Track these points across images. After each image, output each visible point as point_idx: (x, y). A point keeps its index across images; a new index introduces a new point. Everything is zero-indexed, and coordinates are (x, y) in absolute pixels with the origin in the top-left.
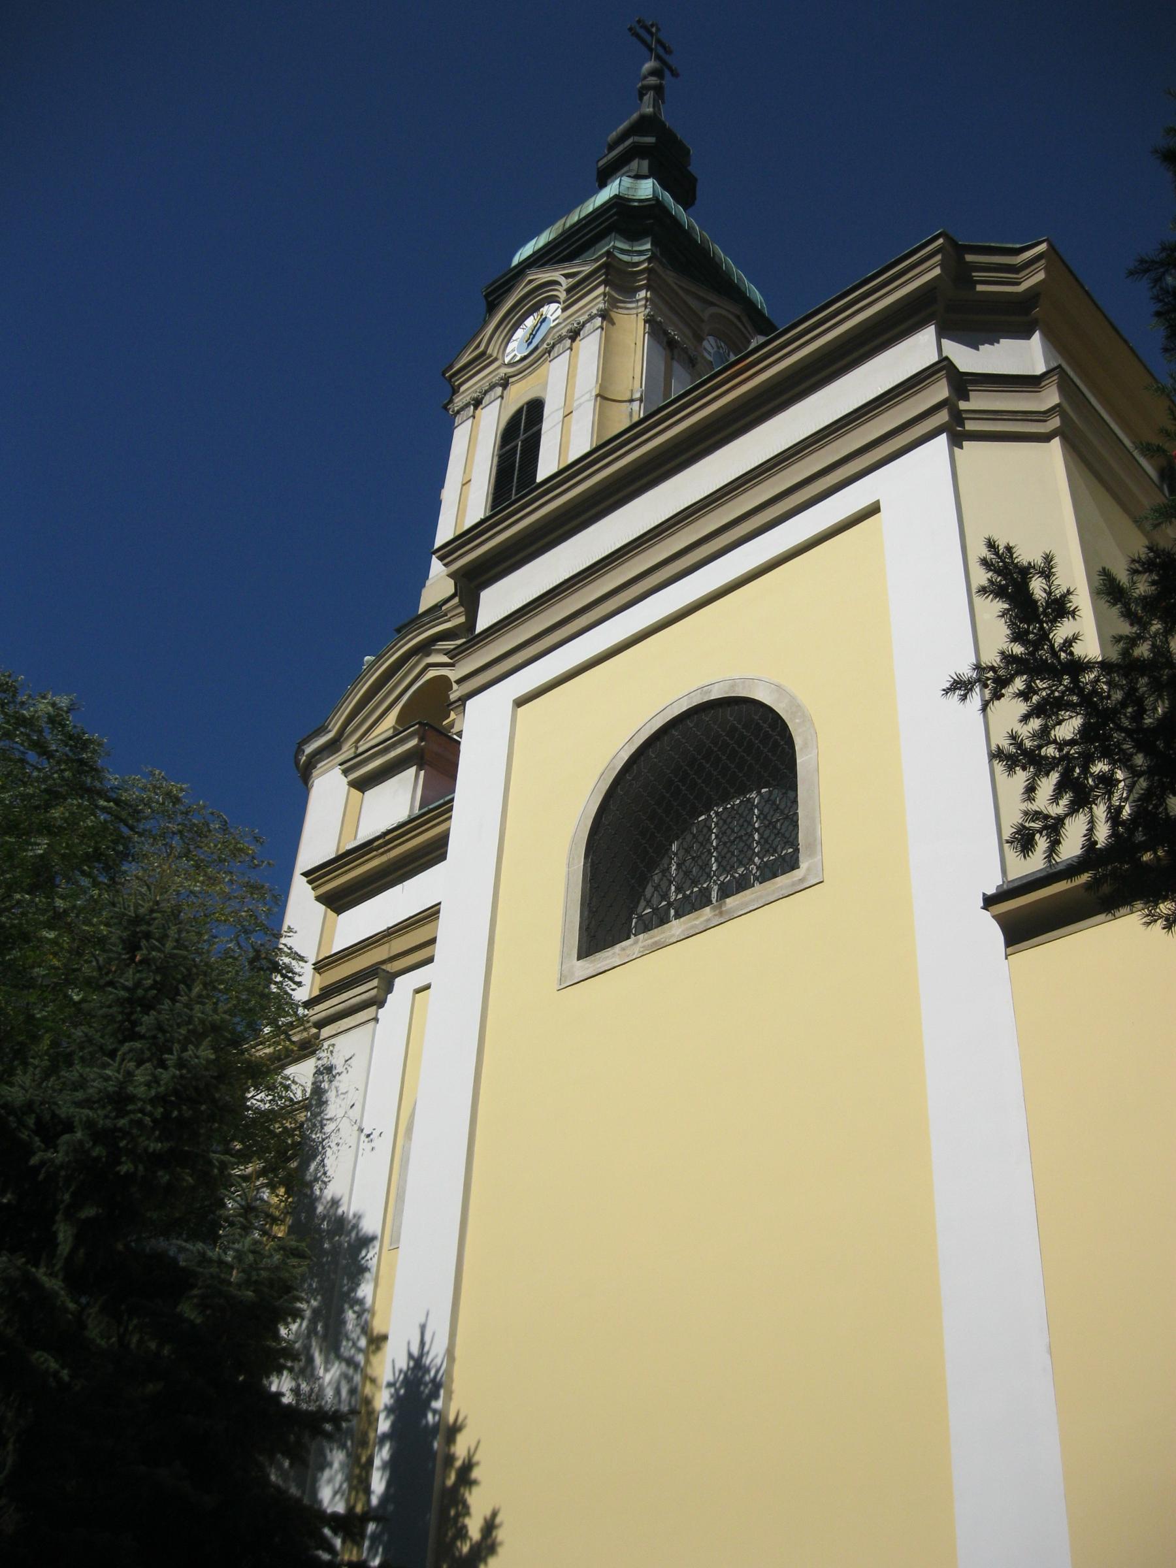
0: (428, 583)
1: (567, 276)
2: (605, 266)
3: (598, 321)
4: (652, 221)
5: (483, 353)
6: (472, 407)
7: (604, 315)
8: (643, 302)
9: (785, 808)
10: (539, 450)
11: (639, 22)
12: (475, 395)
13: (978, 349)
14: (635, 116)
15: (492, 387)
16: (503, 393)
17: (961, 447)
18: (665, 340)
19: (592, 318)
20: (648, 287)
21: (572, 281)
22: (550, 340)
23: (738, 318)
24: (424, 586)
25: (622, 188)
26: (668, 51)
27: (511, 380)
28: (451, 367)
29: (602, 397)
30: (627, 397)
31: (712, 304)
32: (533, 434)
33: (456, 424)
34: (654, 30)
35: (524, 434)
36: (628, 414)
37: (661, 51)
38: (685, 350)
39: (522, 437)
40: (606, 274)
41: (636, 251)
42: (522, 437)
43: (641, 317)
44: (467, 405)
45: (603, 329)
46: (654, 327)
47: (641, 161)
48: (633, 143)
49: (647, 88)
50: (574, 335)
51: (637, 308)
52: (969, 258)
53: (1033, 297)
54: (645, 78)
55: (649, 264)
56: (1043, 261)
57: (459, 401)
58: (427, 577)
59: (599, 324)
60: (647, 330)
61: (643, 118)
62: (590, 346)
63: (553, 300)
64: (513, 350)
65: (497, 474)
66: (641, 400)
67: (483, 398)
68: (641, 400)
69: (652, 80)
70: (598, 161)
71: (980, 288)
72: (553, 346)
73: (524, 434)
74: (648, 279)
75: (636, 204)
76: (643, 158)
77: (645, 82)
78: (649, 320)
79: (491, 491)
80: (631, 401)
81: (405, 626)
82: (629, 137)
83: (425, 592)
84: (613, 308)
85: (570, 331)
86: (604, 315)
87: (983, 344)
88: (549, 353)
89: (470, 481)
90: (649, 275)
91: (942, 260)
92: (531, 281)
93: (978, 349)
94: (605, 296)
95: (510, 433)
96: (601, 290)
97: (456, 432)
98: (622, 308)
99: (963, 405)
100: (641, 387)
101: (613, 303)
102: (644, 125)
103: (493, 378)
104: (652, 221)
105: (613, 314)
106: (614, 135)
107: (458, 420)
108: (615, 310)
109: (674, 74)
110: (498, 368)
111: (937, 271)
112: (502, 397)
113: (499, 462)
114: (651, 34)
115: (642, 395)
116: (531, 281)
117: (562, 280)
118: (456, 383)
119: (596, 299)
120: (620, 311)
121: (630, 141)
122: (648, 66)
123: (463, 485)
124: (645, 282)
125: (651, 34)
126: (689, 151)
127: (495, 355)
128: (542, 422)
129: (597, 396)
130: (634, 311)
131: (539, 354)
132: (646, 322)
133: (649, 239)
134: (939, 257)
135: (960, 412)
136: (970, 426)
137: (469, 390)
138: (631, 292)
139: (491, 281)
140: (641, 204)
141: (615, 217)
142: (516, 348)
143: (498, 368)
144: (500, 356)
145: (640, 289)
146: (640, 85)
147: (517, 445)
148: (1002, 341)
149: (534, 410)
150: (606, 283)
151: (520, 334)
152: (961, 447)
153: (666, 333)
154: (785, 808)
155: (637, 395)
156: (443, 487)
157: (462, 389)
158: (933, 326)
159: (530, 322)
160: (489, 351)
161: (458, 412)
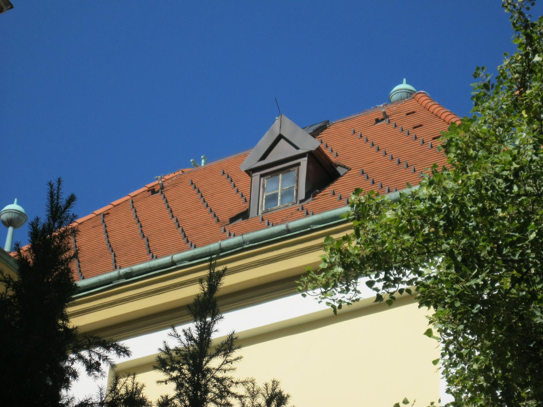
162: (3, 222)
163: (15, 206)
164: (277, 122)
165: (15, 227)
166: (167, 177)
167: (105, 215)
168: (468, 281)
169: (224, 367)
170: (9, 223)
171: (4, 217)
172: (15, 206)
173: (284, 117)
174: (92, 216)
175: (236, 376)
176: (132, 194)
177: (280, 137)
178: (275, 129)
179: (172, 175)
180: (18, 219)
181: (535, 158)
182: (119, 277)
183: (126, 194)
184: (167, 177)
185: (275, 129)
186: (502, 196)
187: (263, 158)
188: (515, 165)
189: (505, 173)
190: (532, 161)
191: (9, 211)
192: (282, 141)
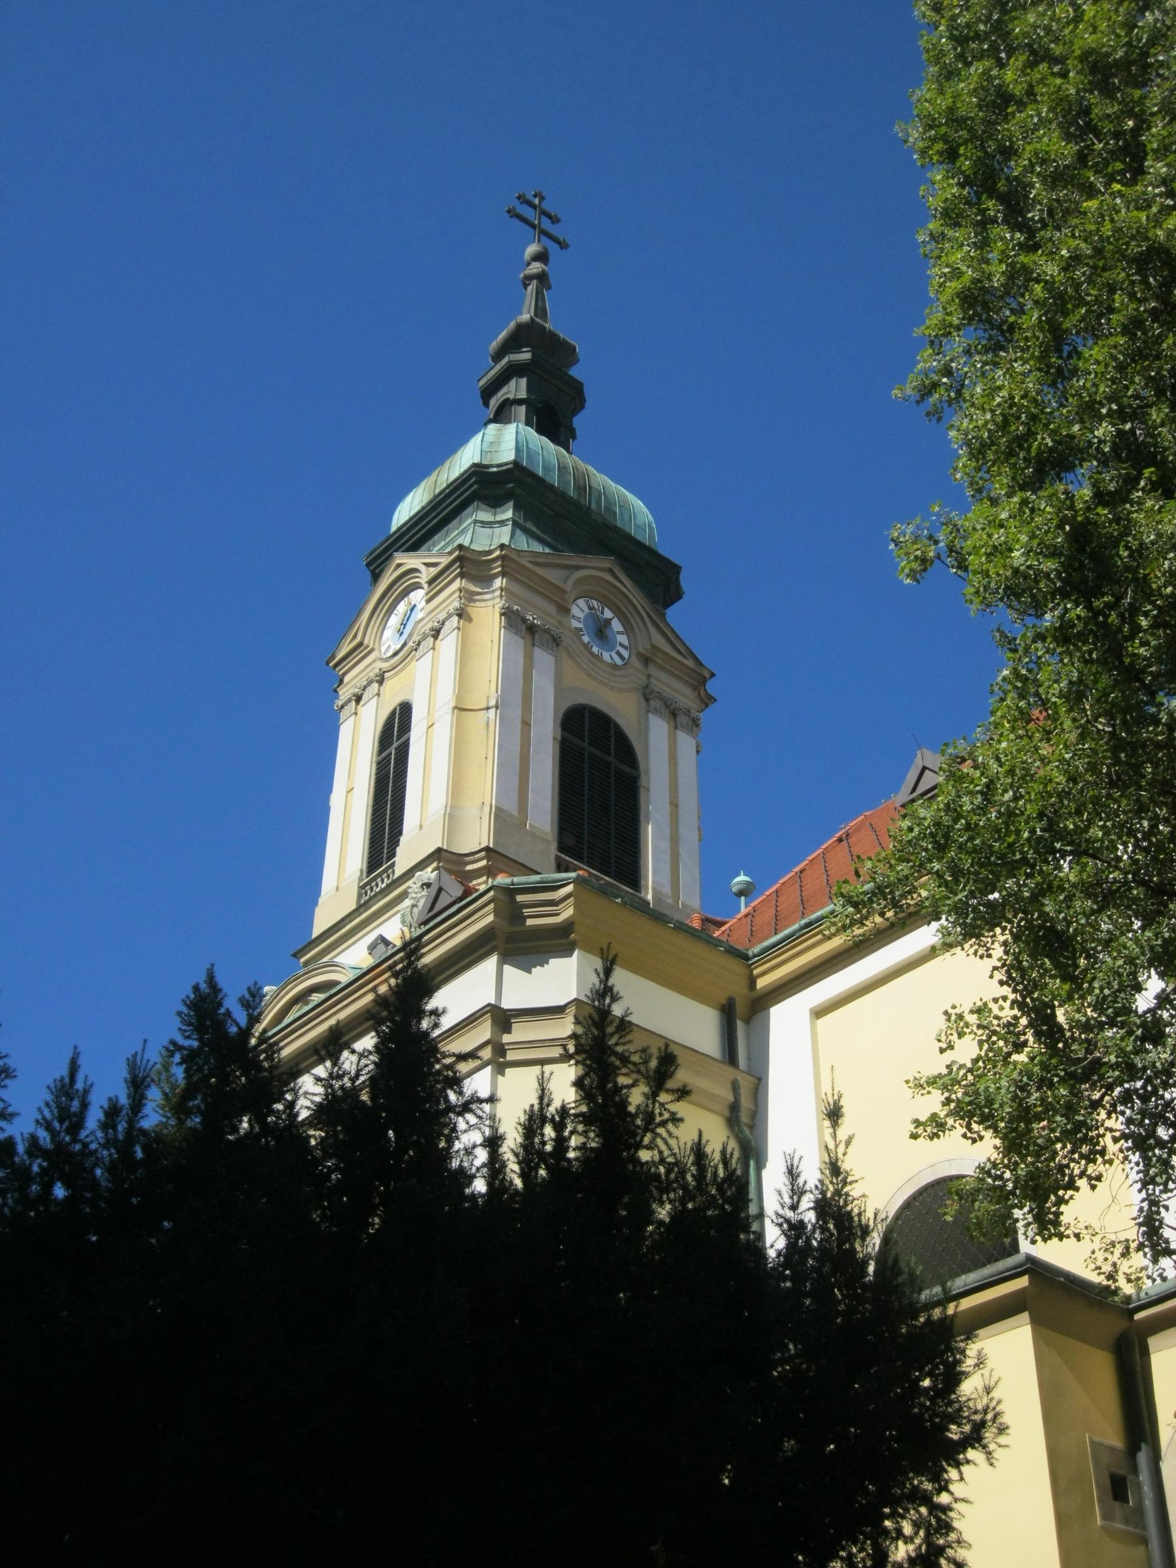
0: (321, 900)
1: (427, 565)
2: (459, 559)
3: (455, 618)
4: (512, 485)
5: (360, 644)
6: (354, 703)
7: (461, 614)
8: (498, 593)
9: (668, 1131)
10: (407, 763)
11: (519, 198)
12: (357, 690)
13: (530, 972)
14: (512, 324)
15: (370, 683)
16: (379, 690)
17: (503, 1075)
18: (524, 627)
19: (450, 616)
20: (503, 574)
21: (434, 571)
22: (416, 638)
23: (611, 571)
24: (316, 904)
25: (485, 444)
26: (554, 220)
27: (387, 675)
28: (333, 657)
29: (459, 709)
30: (483, 705)
31: (578, 568)
32: (403, 743)
33: (341, 721)
34: (537, 201)
35: (397, 740)
36: (485, 723)
37: (546, 224)
38: (547, 631)
39: (395, 745)
40: (461, 567)
41: (498, 522)
42: (395, 745)
43: (497, 611)
44: (350, 700)
45: (459, 629)
46: (512, 619)
47: (519, 380)
48: (509, 361)
49: (528, 279)
50: (436, 633)
51: (493, 599)
52: (519, 898)
53: (566, 929)
54: (529, 264)
55: (501, 551)
56: (572, 899)
57: (345, 693)
58: (319, 895)
59: (456, 625)
60: (503, 624)
61: (520, 327)
62: (449, 643)
63: (417, 586)
64: (388, 640)
65: (376, 783)
66: (497, 707)
67: (362, 694)
68: (497, 707)
69: (536, 267)
70: (479, 380)
71: (530, 922)
72: (419, 644)
73: (397, 740)
74: (503, 566)
75: (495, 469)
76: (521, 377)
77: (527, 272)
78: (507, 613)
79: (371, 803)
80: (488, 708)
81: (300, 951)
82: (504, 357)
83: (318, 912)
84: (470, 602)
85: (432, 629)
86: (461, 614)
87: (535, 967)
88: (416, 650)
89: (352, 789)
90: (503, 562)
91: (495, 908)
92: (399, 565)
93: (530, 972)
94: (461, 591)
95: (385, 738)
96: (457, 584)
97: (342, 727)
98: (479, 601)
99: (506, 1039)
100: (497, 692)
101: (468, 597)
102: (519, 337)
103: (370, 671)
104: (512, 485)
105: (469, 610)
106: (494, 345)
107: (343, 715)
108: (472, 604)
109: (563, 245)
110: (374, 661)
111: (491, 918)
112: (378, 694)
113: (377, 769)
114: (534, 207)
115: (497, 702)
116: (399, 565)
117: (423, 568)
118: (341, 673)
119: (450, 597)
120: (477, 604)
121: (505, 361)
122: (532, 249)
123: (348, 792)
124: (500, 569)
125: (534, 207)
126: (575, 348)
127: (371, 646)
128: (410, 730)
129: (455, 708)
130: (491, 603)
131: (405, 654)
132: (502, 614)
133: (511, 504)
134: (492, 906)
135: (503, 1045)
136: (511, 1056)
137: (354, 679)
138: (487, 580)
139: (369, 552)
140: (500, 469)
141: (476, 486)
142: (390, 640)
143: (374, 661)
144: (376, 646)
145: (495, 576)
146: (522, 275)
147: (391, 754)
148: (551, 961)
149: (405, 710)
150: (462, 575)
151: (394, 620)
152: (503, 1075)
153: (524, 620)
154: (668, 1131)
155: (493, 703)
156: (331, 791)
157: (347, 679)
158: (496, 957)
159: (402, 607)
160: (366, 642)
161: (342, 707)
162: (735, 894)
163: (742, 878)
164: (919, 755)
165: (746, 896)
166: (852, 824)
167: (801, 872)
168: (956, 895)
169: (621, 1041)
170: (740, 893)
171: (734, 889)
172: (742, 878)
173: (925, 751)
174: (792, 874)
175: (632, 1048)
176: (824, 847)
177: (924, 769)
178: (919, 763)
179: (854, 822)
180: (747, 888)
181: (1000, 769)
182: (802, 928)
183: (819, 848)
184: (852, 824)
185: (919, 763)
186: (981, 808)
187: (432, 908)
188: (984, 780)
189: (978, 788)
190: (998, 772)
191: (738, 883)
192: (927, 771)
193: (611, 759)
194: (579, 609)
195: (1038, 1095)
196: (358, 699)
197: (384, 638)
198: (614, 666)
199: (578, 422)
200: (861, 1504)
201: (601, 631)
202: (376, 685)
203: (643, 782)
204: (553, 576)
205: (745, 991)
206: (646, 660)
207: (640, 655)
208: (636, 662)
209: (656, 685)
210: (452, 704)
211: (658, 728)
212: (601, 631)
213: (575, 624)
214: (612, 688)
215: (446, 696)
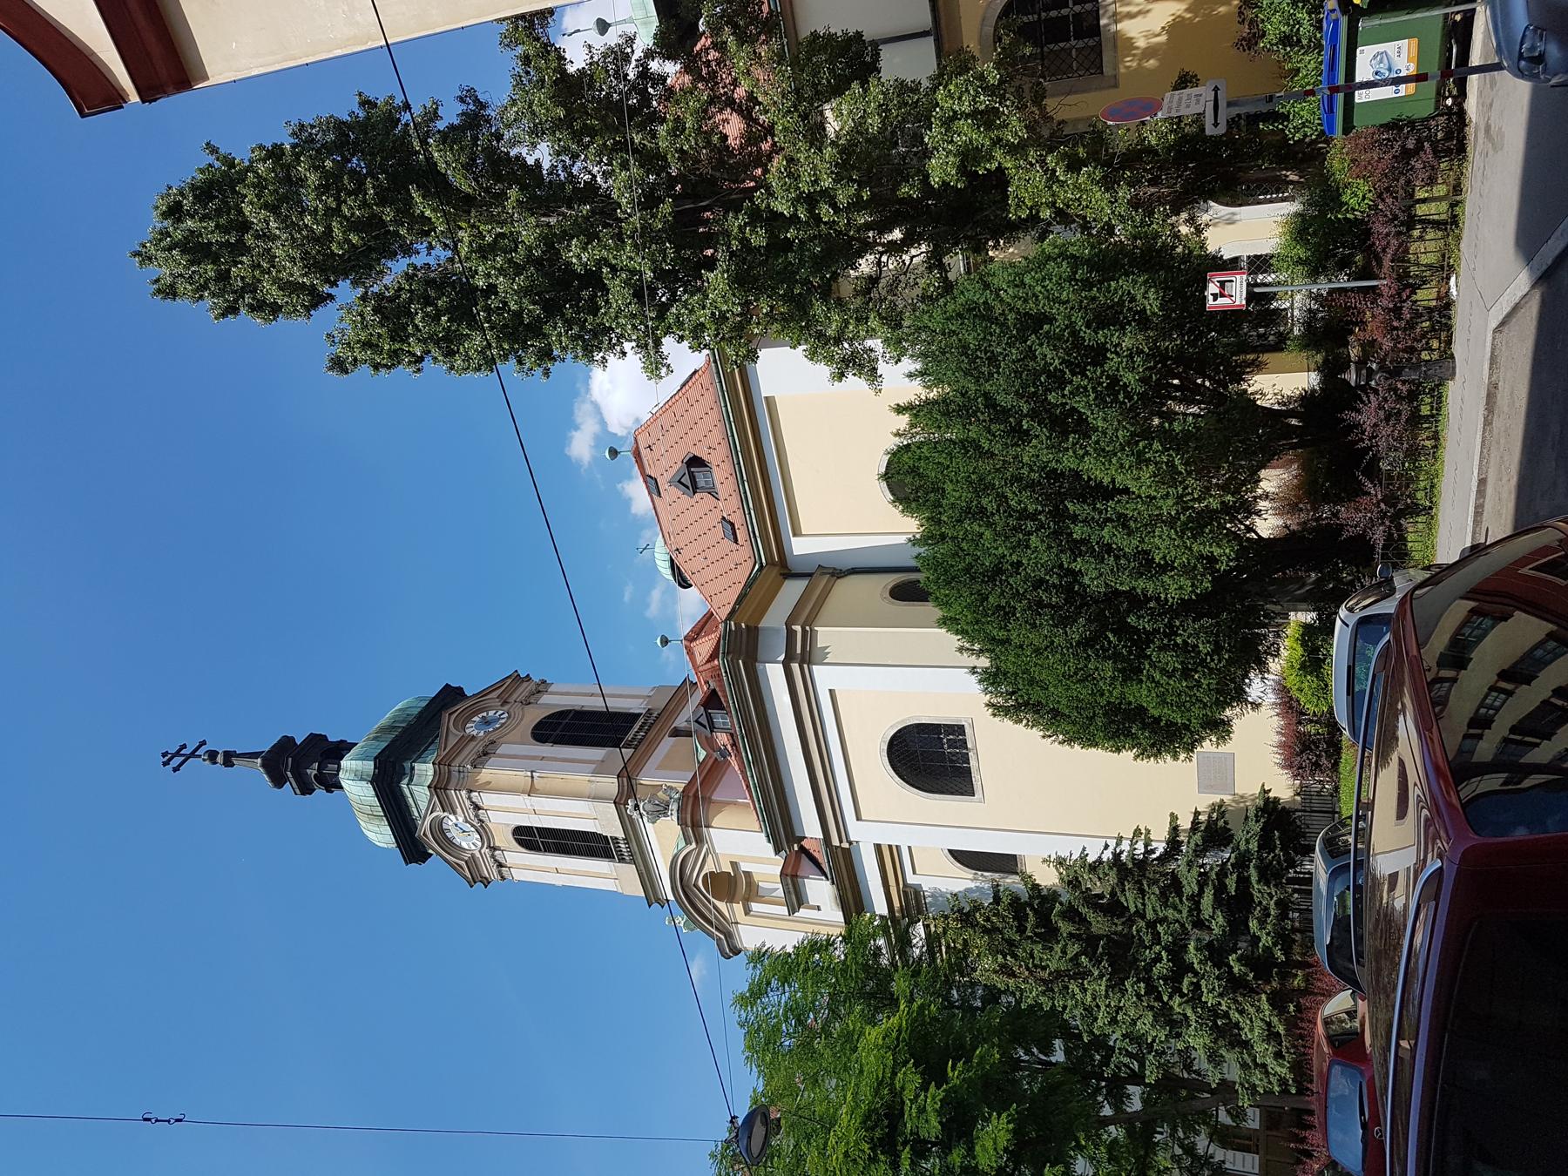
5: (466, 862)
21: (439, 808)
50: (477, 807)
62: (486, 799)
80: (532, 777)
92: (424, 834)
116: (424, 834)
131: (483, 830)
193: (558, 732)
194: (471, 730)
195: (1322, 16)
196: (500, 865)
197: (466, 847)
198: (509, 718)
199: (333, 738)
200: (1027, 1109)
201: (486, 722)
202: (497, 852)
203: (577, 708)
204: (452, 741)
205: (777, 568)
206: (505, 703)
207: (502, 705)
208: (506, 708)
209: (522, 698)
210: (526, 796)
211: (545, 699)
212: (486, 722)
213: (482, 734)
214: (522, 720)
215: (522, 801)
